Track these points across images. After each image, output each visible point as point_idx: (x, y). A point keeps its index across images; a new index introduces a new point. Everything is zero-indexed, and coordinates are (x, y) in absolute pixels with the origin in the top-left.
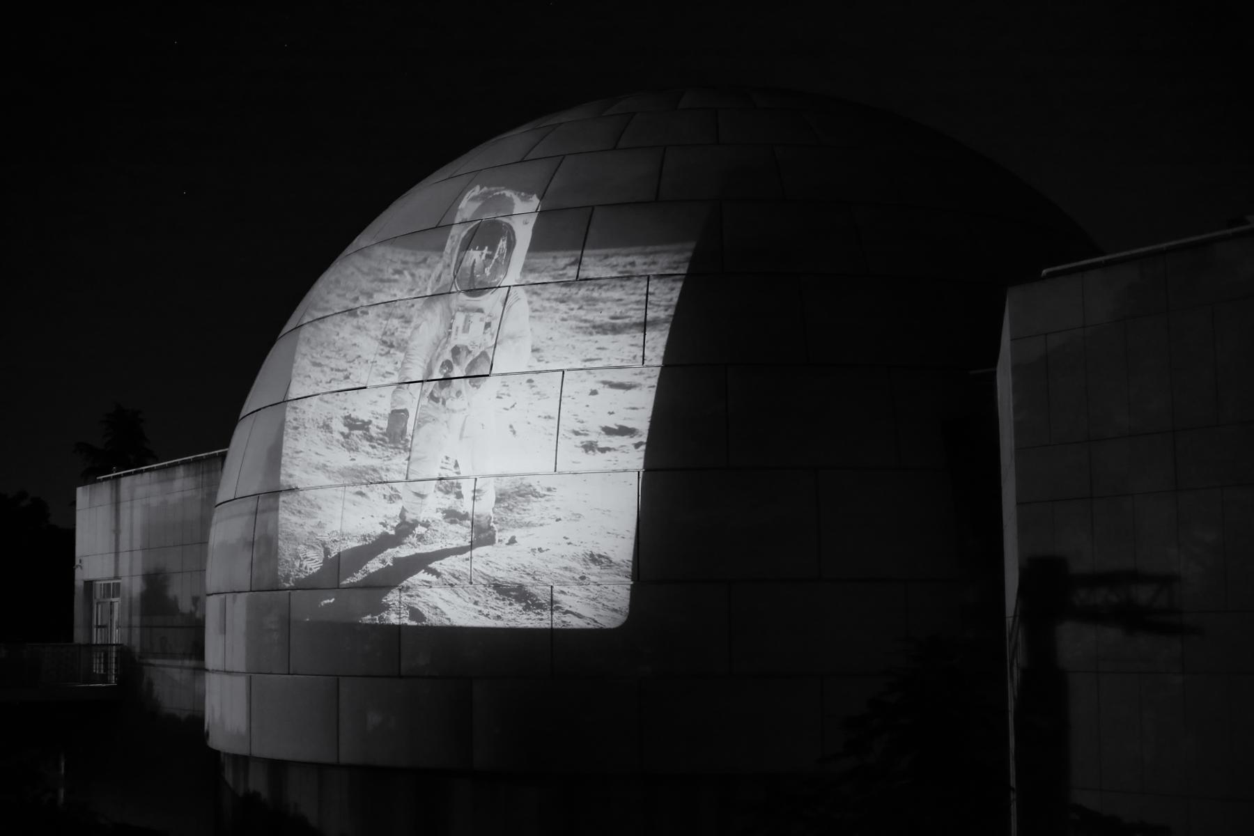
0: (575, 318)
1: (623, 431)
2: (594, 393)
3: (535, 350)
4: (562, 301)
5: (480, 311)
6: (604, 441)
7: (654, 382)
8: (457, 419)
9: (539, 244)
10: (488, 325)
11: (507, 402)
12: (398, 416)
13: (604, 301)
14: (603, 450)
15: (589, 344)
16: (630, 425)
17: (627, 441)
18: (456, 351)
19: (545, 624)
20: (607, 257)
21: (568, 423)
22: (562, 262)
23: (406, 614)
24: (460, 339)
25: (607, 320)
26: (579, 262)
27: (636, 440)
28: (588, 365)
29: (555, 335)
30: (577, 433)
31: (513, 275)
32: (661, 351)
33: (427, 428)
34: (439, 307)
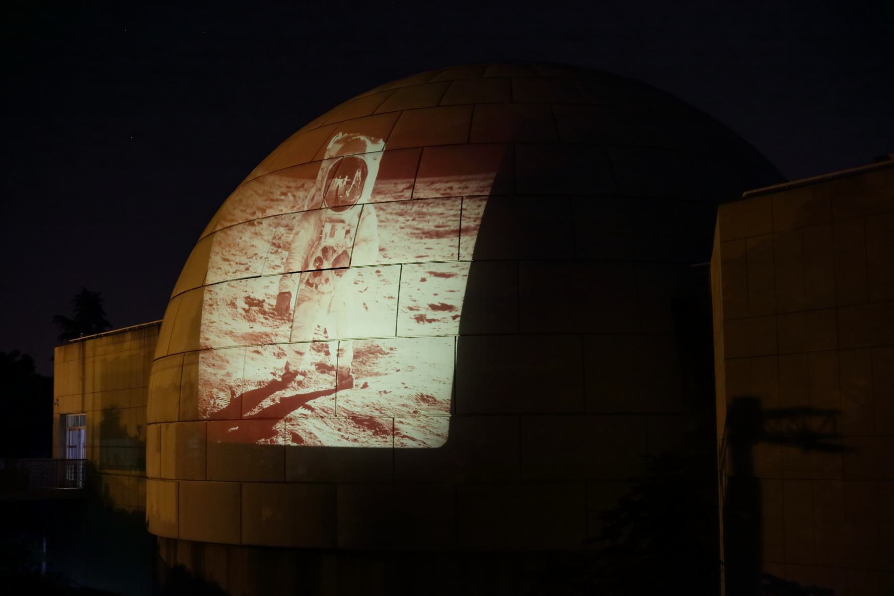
0: (410, 227)
1: (444, 307)
2: (423, 280)
3: (381, 250)
4: (401, 215)
5: (342, 221)
6: (431, 314)
7: (466, 272)
8: (326, 299)
9: (384, 174)
10: (348, 232)
11: (361, 287)
12: (284, 297)
13: (431, 214)
14: (430, 321)
15: (421, 246)
16: (449, 303)
17: (447, 314)
18: (325, 250)
19: (388, 445)
20: (432, 183)
21: (405, 302)
22: (401, 187)
23: (289, 437)
24: (328, 242)
25: (432, 228)
26: (412, 187)
27: (454, 313)
28: (420, 260)
29: (396, 239)
30: (411, 309)
31: (366, 196)
32: (471, 250)
33: (304, 305)
34: (313, 219)
